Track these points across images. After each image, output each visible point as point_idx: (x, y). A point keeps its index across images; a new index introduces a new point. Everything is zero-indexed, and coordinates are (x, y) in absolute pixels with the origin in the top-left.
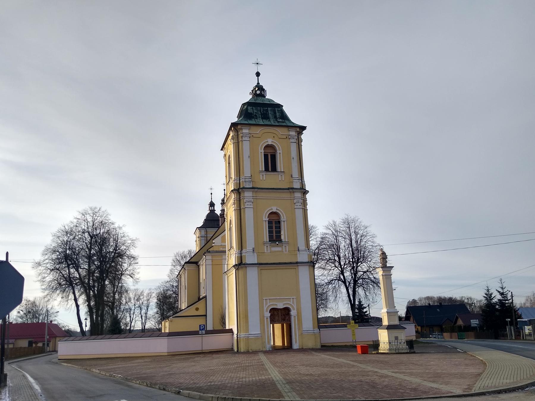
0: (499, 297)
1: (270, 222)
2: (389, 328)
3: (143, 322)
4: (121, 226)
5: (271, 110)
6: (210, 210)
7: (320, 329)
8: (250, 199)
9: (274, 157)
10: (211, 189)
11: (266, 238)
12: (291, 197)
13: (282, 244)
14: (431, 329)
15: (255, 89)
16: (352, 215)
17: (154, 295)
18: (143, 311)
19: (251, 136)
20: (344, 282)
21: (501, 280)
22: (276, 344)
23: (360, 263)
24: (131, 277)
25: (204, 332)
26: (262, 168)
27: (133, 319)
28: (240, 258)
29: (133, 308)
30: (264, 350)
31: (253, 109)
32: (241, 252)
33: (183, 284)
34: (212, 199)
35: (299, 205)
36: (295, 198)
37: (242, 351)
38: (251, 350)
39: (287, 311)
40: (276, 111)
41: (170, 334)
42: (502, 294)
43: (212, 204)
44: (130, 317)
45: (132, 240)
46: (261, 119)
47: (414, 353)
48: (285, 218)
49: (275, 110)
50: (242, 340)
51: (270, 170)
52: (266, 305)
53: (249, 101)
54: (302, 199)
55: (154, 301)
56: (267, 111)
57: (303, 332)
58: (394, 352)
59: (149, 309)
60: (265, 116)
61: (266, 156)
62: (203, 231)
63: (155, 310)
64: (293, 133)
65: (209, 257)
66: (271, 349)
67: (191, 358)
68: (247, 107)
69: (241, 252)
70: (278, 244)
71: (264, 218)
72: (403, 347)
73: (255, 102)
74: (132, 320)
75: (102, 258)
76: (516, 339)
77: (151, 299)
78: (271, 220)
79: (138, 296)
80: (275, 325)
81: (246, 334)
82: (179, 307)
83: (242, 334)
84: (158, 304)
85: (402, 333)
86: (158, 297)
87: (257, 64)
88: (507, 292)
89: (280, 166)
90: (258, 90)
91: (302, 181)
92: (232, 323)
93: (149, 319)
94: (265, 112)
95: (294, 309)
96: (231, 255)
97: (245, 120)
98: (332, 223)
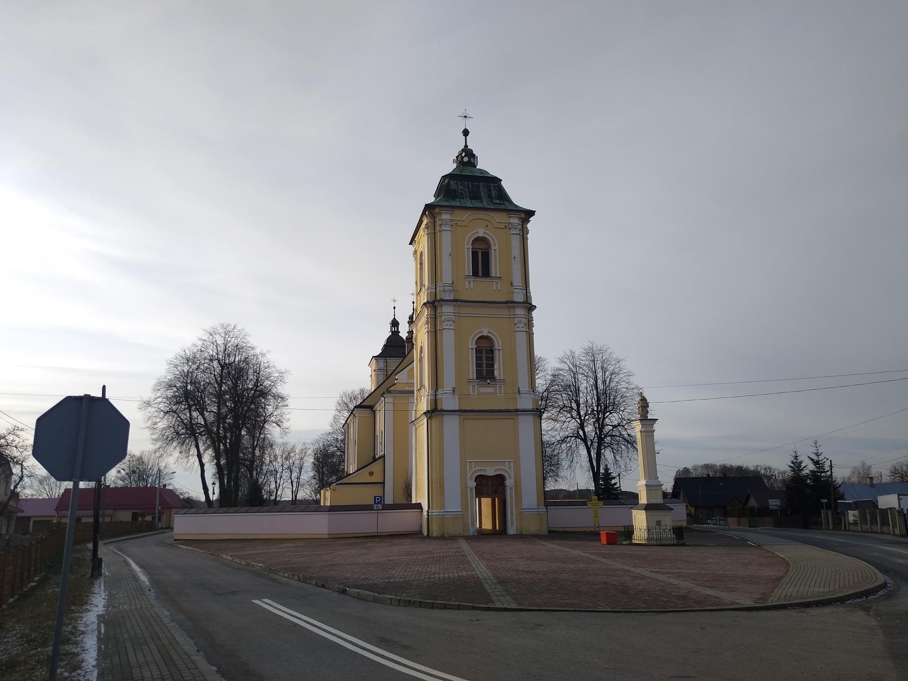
0: (812, 467)
1: (478, 351)
3: (294, 489)
4: (264, 351)
6: (392, 332)
7: (548, 507)
8: (451, 317)
9: (486, 255)
10: (394, 301)
11: (472, 373)
12: (510, 315)
13: (495, 383)
15: (462, 154)
17: (310, 452)
18: (295, 475)
19: (454, 224)
20: (585, 440)
21: (816, 443)
22: (483, 527)
23: (608, 413)
24: (278, 425)
25: (380, 506)
30: (466, 534)
32: (436, 392)
33: (352, 438)
34: (394, 315)
35: (521, 327)
36: (516, 316)
37: (434, 535)
40: (492, 188)
41: (332, 509)
42: (816, 463)
43: (395, 323)
44: (276, 482)
46: (469, 199)
47: (684, 545)
48: (501, 345)
49: (490, 186)
51: (480, 274)
52: (471, 469)
54: (525, 318)
55: (309, 461)
56: (478, 187)
57: (523, 511)
58: (655, 543)
60: (475, 196)
62: (382, 362)
63: (312, 474)
64: (515, 221)
65: (389, 399)
66: (476, 534)
68: (448, 181)
69: (436, 392)
70: (489, 383)
71: (470, 344)
72: (668, 536)
74: (278, 486)
76: (834, 529)
78: (481, 348)
79: (287, 453)
81: (441, 511)
83: (435, 512)
84: (315, 464)
85: (667, 517)
88: (824, 461)
89: (495, 270)
90: (465, 156)
92: (420, 496)
93: (303, 486)
94: (475, 189)
95: (510, 477)
98: (569, 354)
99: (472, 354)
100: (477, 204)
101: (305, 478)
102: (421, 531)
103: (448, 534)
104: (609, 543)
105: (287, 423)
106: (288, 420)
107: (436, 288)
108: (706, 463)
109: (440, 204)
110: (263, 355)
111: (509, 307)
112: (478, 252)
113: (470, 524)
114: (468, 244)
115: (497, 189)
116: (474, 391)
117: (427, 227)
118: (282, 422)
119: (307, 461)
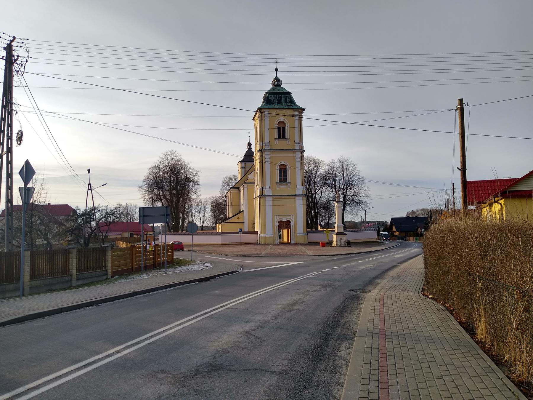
2: (338, 234)
3: (202, 222)
4: (189, 162)
5: (283, 97)
6: (248, 148)
9: (284, 129)
11: (277, 179)
14: (407, 234)
15: (274, 80)
16: (345, 156)
17: (209, 203)
18: (202, 214)
22: (284, 241)
23: (349, 190)
24: (195, 194)
25: (241, 232)
26: (276, 137)
27: (194, 220)
28: (262, 192)
29: (194, 212)
30: (275, 243)
31: (272, 96)
33: (230, 201)
37: (262, 244)
38: (267, 243)
39: (288, 223)
40: (287, 97)
41: (222, 233)
43: (249, 144)
44: (192, 218)
45: (197, 172)
46: (277, 104)
47: (350, 247)
50: (262, 238)
52: (276, 218)
53: (270, 91)
55: (209, 208)
56: (281, 97)
58: (338, 246)
59: (205, 213)
60: (279, 102)
61: (279, 129)
62: (243, 164)
63: (210, 214)
64: (296, 113)
65: (246, 186)
67: (234, 246)
68: (268, 95)
73: (273, 91)
74: (193, 220)
75: (178, 183)
77: (207, 206)
78: (281, 169)
79: (197, 203)
80: (361, 221)
82: (228, 215)
83: (262, 235)
84: (212, 209)
86: (212, 204)
87: (276, 62)
89: (287, 135)
90: (276, 82)
91: (301, 144)
92: (257, 229)
93: (206, 220)
94: (279, 98)
95: (292, 221)
96: (257, 188)
97: (267, 105)
99: (278, 172)
100: (280, 106)
101: (207, 216)
102: (258, 242)
103: (267, 243)
104: (322, 246)
105: (200, 193)
106: (200, 191)
107: (262, 144)
108: (423, 208)
109: (264, 107)
110: (189, 164)
111: (293, 152)
112: (280, 127)
113: (276, 239)
114: (276, 124)
115: (289, 98)
116: (278, 187)
117: (259, 117)
118: (197, 192)
119: (208, 207)
